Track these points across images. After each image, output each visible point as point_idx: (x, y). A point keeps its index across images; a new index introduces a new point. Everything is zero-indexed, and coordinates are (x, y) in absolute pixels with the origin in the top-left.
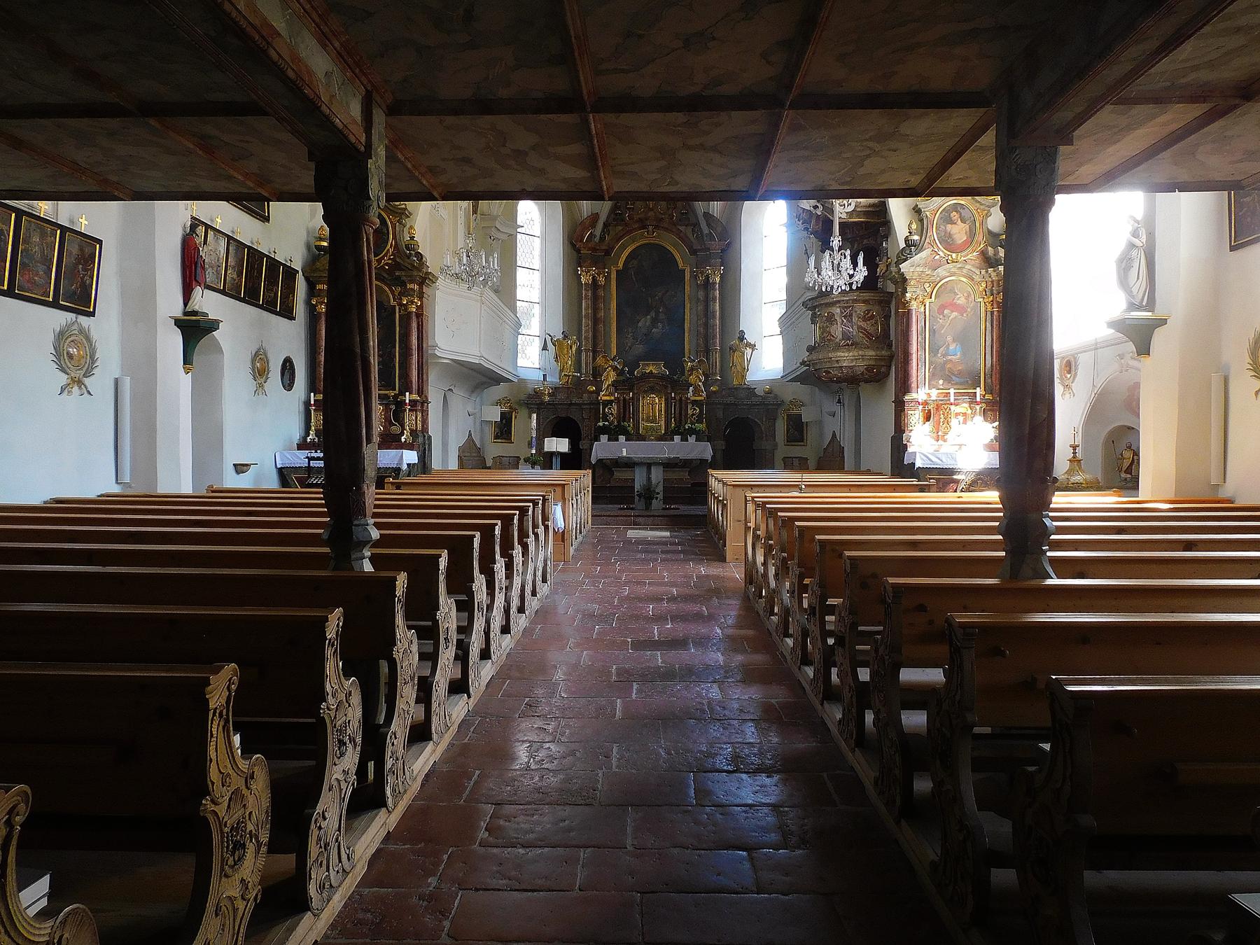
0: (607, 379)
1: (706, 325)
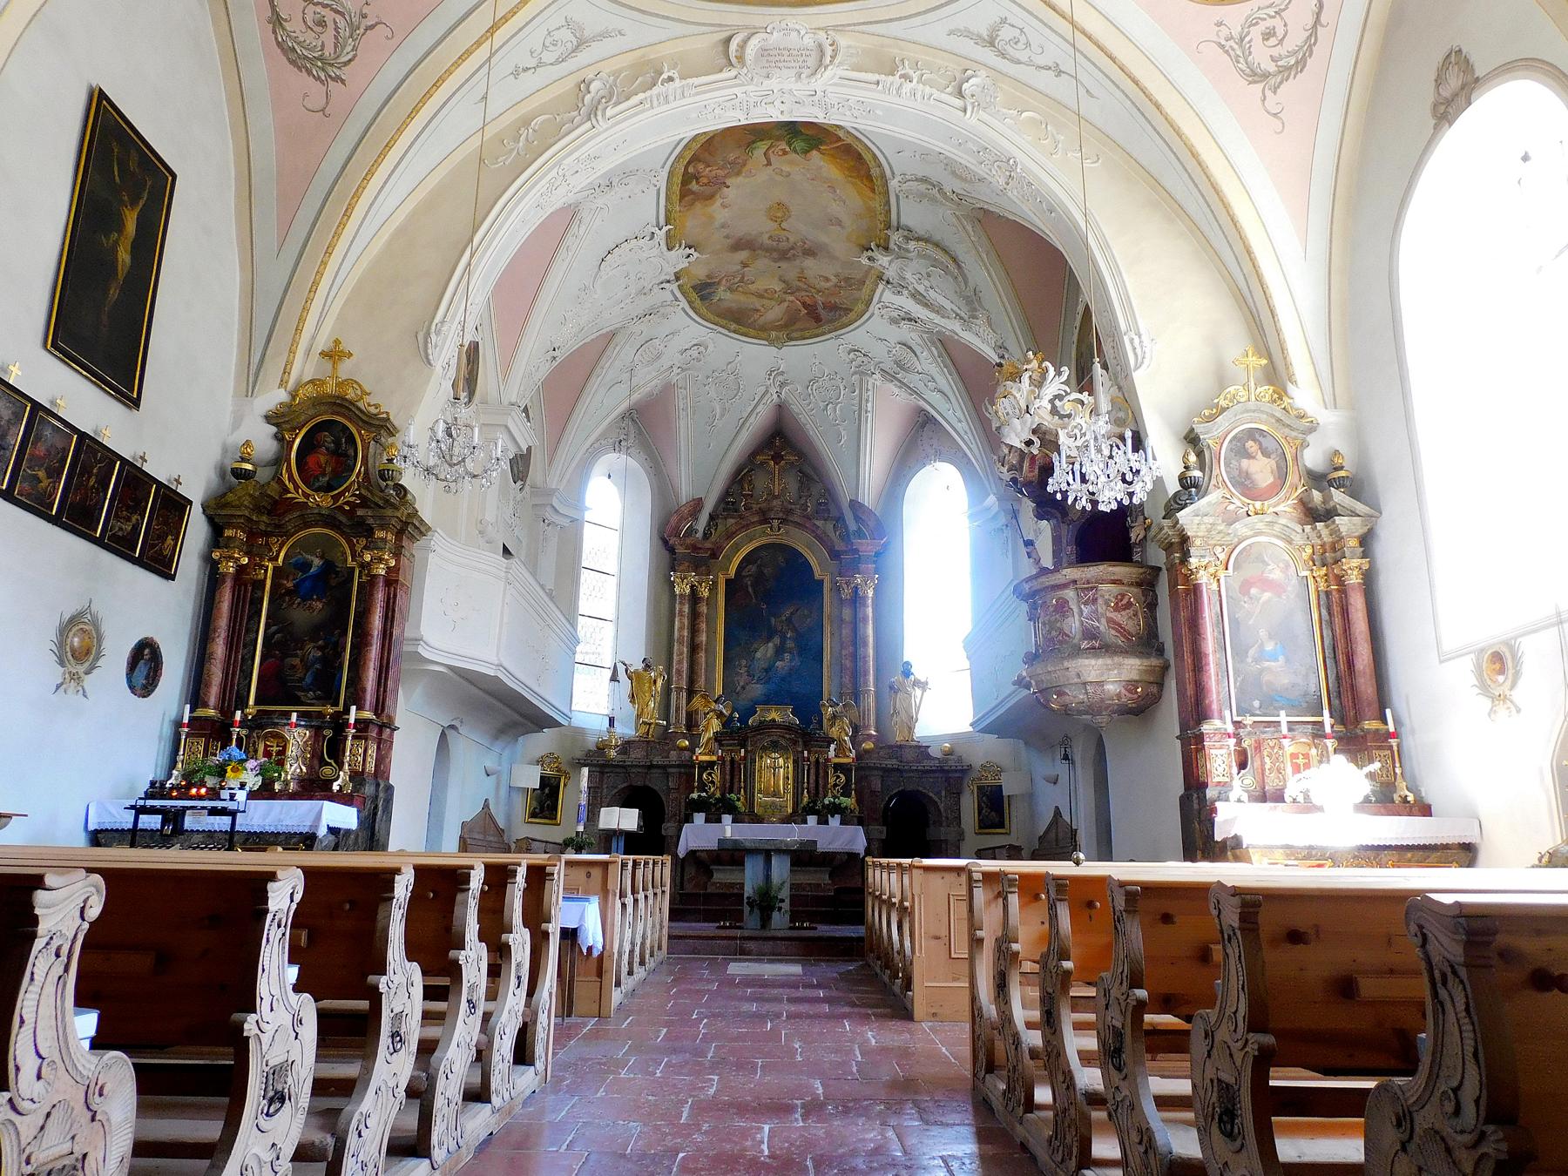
0: (706, 729)
1: (854, 657)
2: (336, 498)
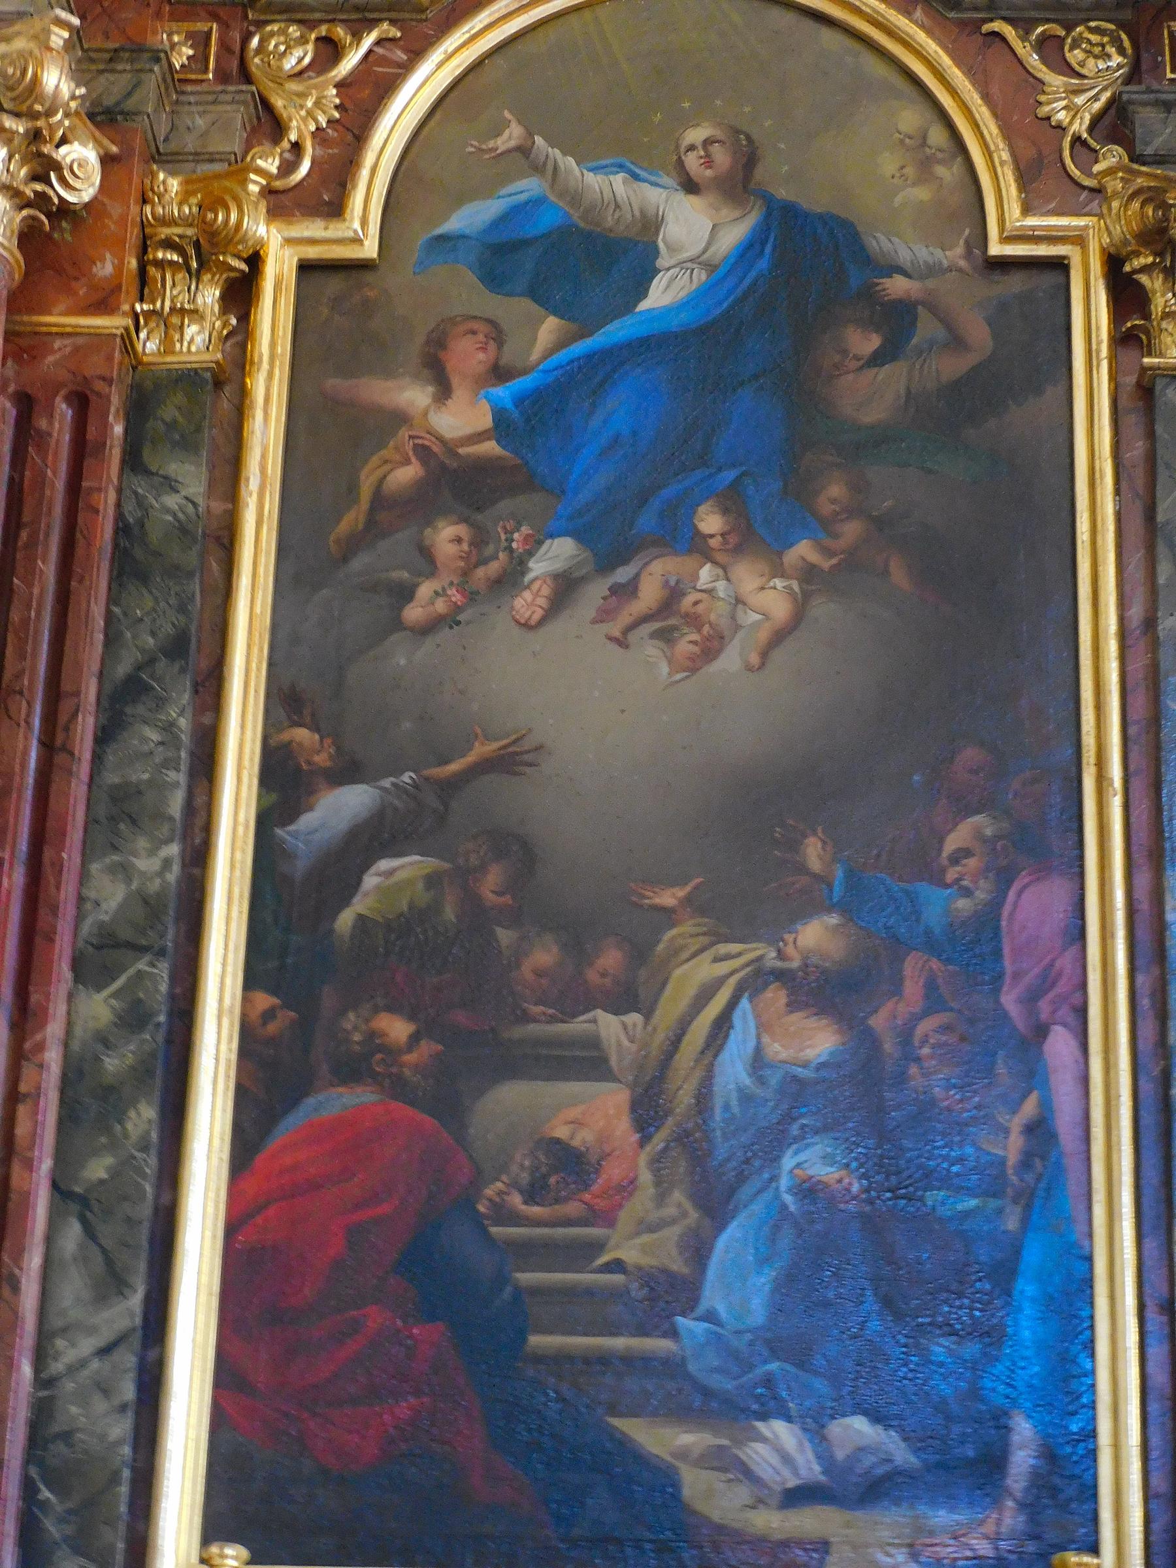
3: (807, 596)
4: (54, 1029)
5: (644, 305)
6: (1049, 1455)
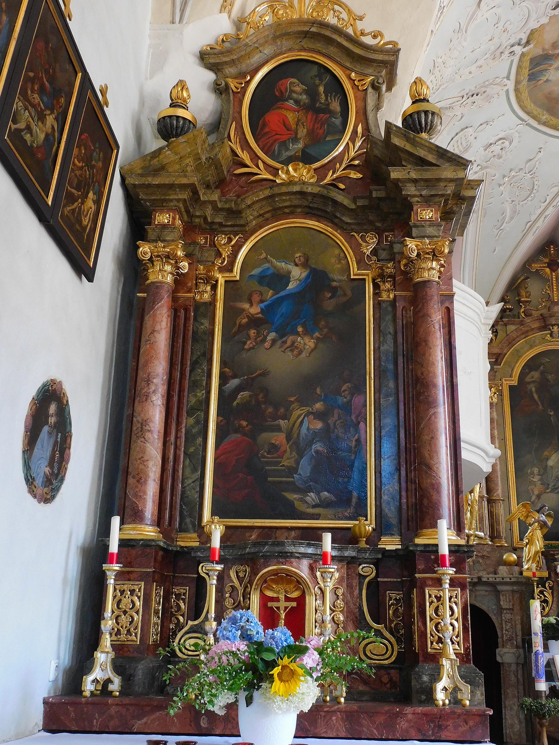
2: (321, 172)
3: (317, 343)
4: (184, 425)
5: (288, 288)
6: (359, 498)
